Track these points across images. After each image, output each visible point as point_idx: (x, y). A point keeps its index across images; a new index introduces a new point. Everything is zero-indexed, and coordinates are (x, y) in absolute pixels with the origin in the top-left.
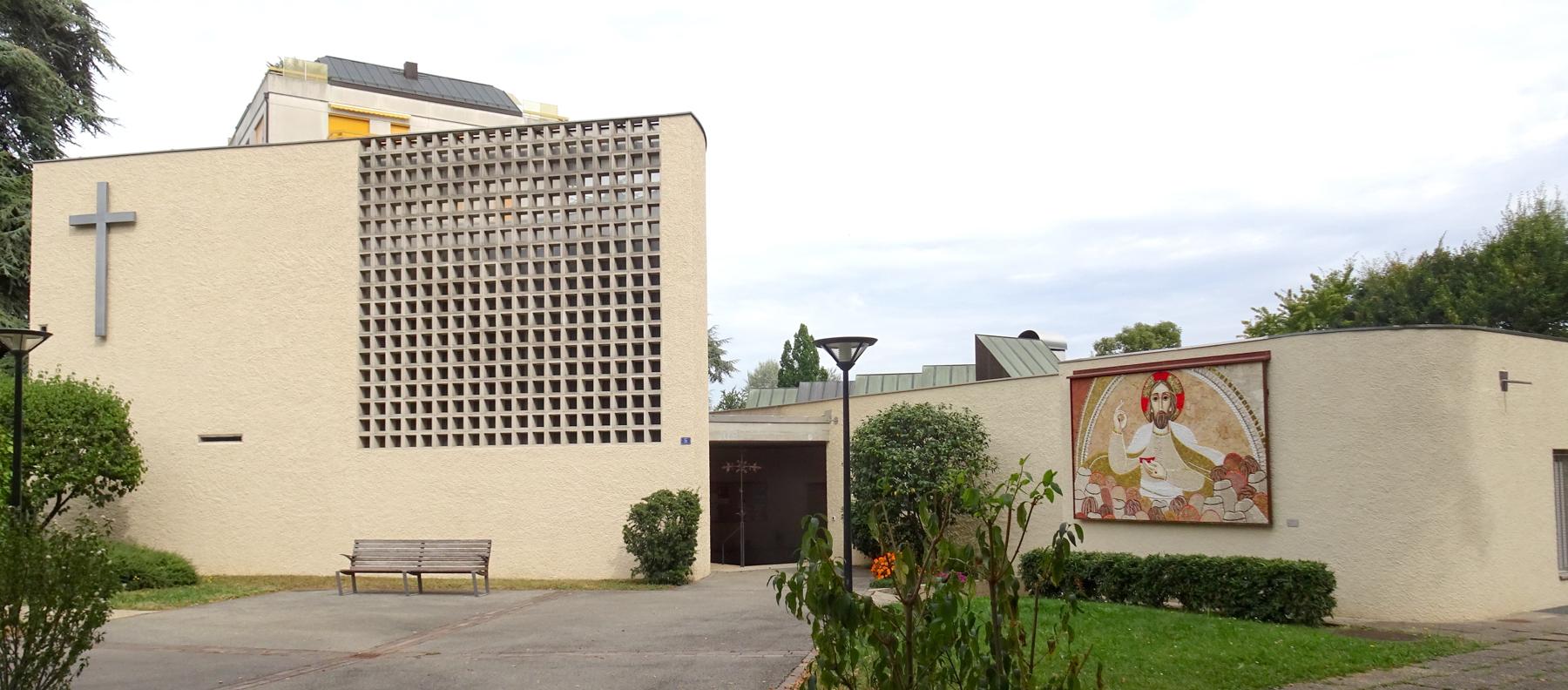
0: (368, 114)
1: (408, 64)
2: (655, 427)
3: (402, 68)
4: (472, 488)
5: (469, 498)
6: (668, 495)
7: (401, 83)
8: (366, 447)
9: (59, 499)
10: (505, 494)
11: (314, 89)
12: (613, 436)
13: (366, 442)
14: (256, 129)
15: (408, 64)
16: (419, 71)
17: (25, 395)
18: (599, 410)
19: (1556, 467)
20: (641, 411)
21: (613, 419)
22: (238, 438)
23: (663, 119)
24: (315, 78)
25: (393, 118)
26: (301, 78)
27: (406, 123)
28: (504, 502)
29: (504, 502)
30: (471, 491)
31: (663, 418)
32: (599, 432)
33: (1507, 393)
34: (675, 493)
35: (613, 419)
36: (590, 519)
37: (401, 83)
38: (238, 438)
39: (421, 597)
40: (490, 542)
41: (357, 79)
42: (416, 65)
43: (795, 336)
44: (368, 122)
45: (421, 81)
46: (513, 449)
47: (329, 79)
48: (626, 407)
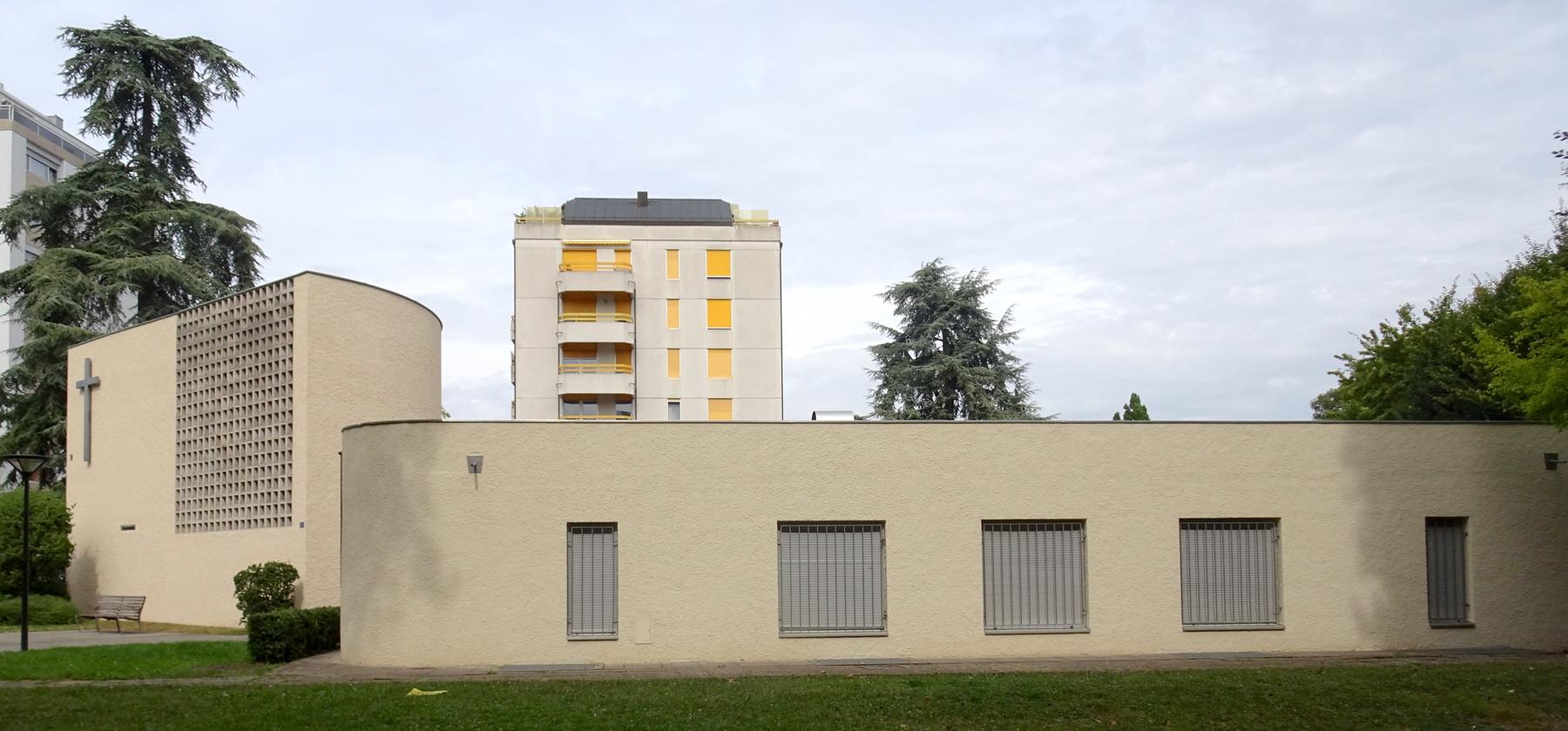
0: (595, 245)
1: (640, 194)
3: (636, 197)
7: (639, 213)
11: (550, 231)
15: (640, 194)
16: (649, 197)
17: (30, 495)
19: (1184, 539)
22: (132, 528)
23: (298, 278)
24: (555, 221)
25: (616, 245)
26: (540, 223)
27: (626, 248)
33: (478, 475)
37: (639, 213)
38: (132, 528)
39: (119, 635)
40: (145, 598)
41: (599, 215)
42: (646, 193)
43: (1126, 407)
44: (595, 251)
45: (649, 207)
47: (563, 219)
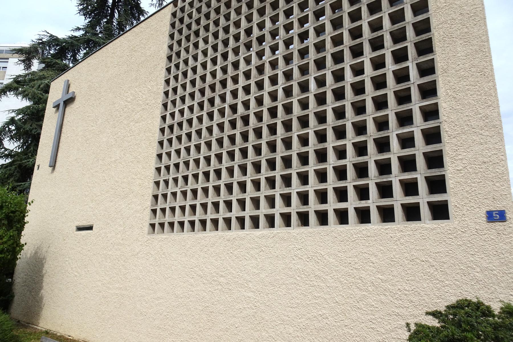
2: (437, 198)
4: (222, 276)
5: (220, 287)
6: (484, 314)
8: (288, 206)
9: (462, 322)
10: (250, 285)
12: (374, 214)
13: (153, 226)
14: (53, 165)
18: (354, 180)
20: (415, 176)
21: (373, 191)
22: (90, 228)
28: (250, 294)
29: (250, 294)
30: (222, 279)
31: (450, 184)
32: (355, 208)
34: (496, 308)
35: (373, 191)
36: (346, 330)
38: (90, 228)
46: (261, 233)
48: (390, 173)
